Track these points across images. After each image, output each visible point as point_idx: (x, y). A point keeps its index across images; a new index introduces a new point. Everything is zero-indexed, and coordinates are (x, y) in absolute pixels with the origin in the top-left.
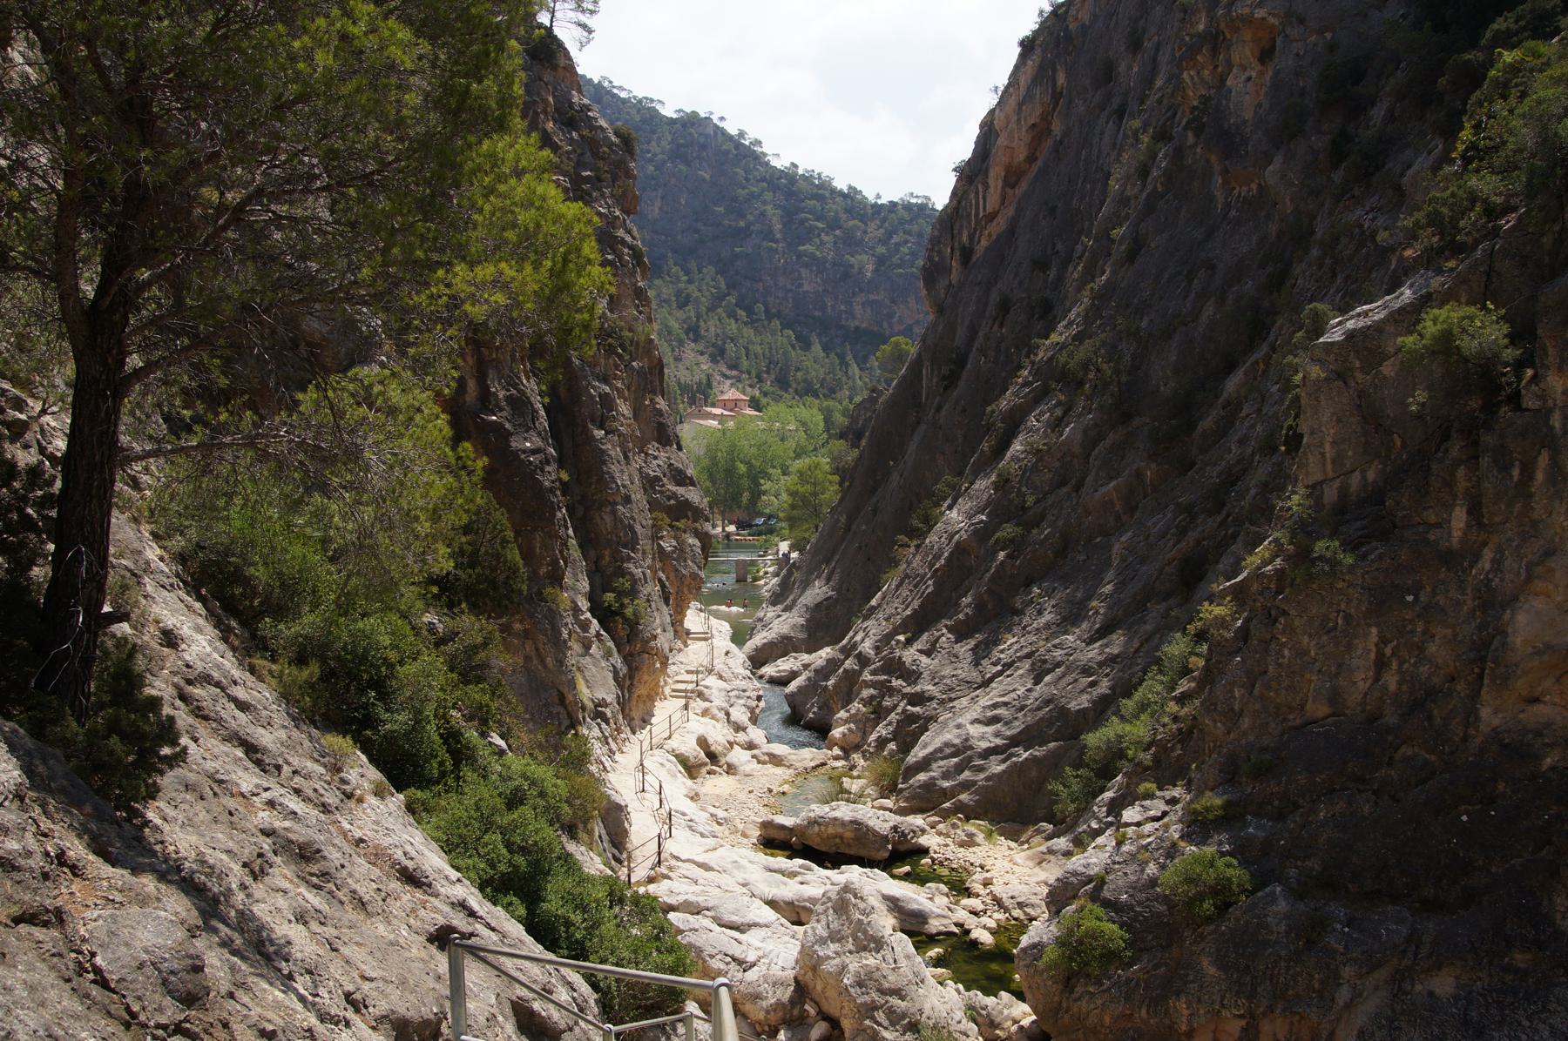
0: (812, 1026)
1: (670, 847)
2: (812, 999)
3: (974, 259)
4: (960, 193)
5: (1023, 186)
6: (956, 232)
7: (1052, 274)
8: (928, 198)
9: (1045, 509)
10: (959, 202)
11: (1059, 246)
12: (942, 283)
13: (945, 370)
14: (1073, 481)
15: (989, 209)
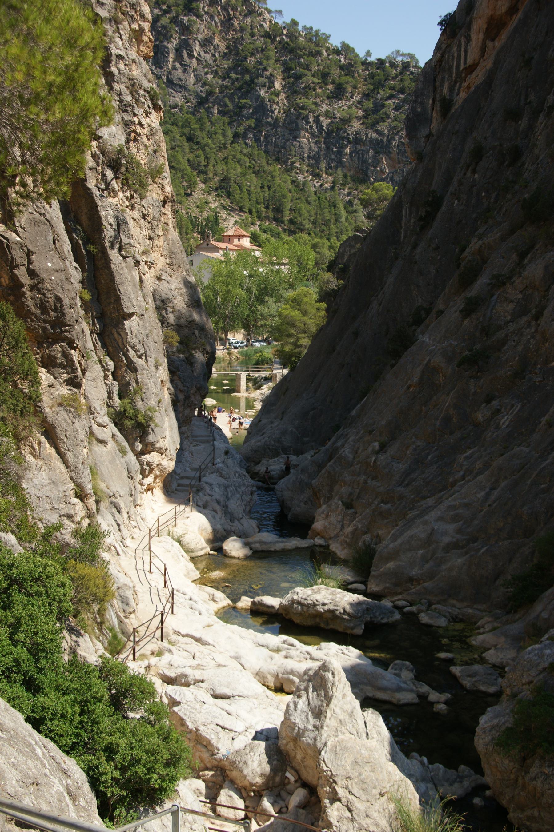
0: (291, 794)
1: (170, 623)
2: (292, 768)
3: (453, 111)
4: (444, 46)
5: (504, 36)
6: (438, 84)
7: (523, 123)
8: (412, 56)
9: (507, 335)
10: (442, 55)
11: (532, 97)
12: (424, 132)
13: (422, 212)
14: (533, 311)
15: (469, 61)
